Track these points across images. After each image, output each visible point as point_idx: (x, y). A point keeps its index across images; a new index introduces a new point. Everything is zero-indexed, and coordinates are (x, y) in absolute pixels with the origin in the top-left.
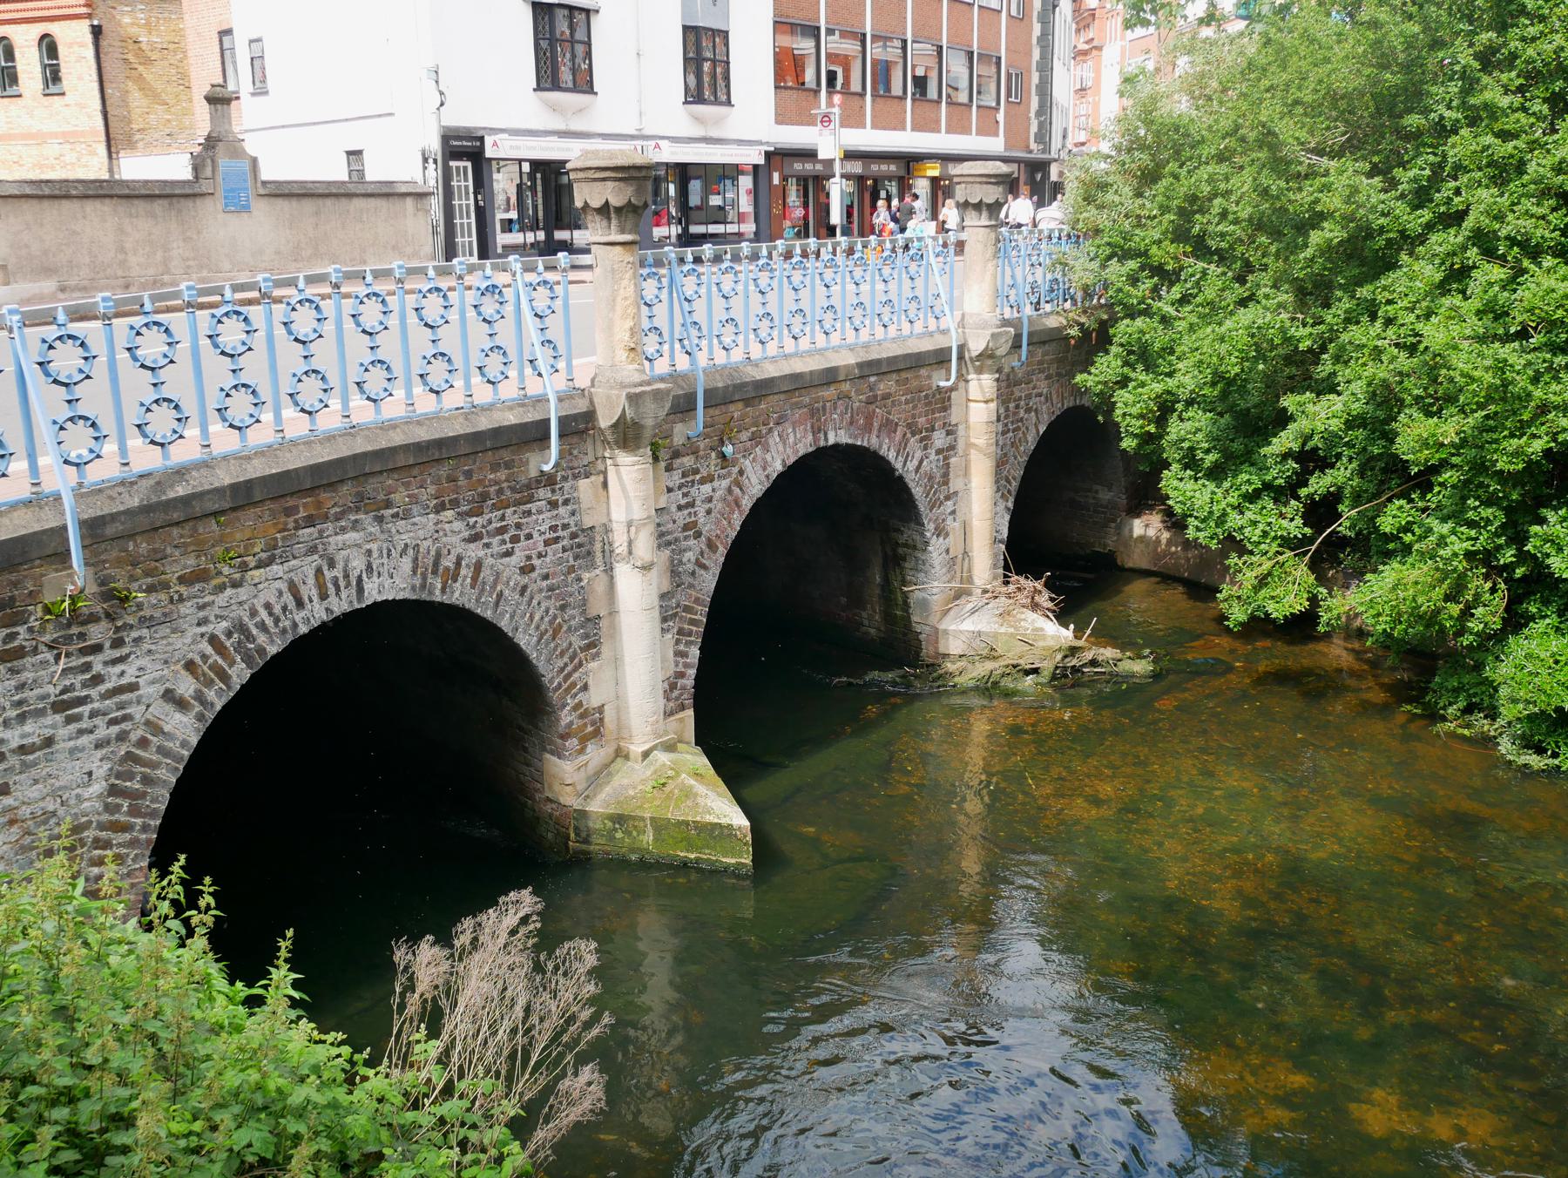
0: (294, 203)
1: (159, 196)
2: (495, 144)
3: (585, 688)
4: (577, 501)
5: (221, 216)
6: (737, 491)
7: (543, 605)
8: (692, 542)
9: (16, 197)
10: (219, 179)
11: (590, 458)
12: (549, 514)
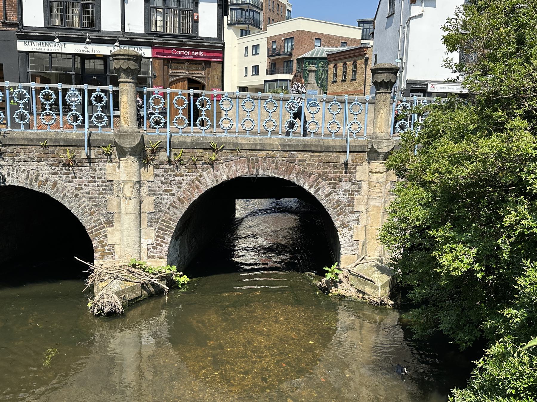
3: (106, 236)
4: (105, 170)
12: (90, 172)
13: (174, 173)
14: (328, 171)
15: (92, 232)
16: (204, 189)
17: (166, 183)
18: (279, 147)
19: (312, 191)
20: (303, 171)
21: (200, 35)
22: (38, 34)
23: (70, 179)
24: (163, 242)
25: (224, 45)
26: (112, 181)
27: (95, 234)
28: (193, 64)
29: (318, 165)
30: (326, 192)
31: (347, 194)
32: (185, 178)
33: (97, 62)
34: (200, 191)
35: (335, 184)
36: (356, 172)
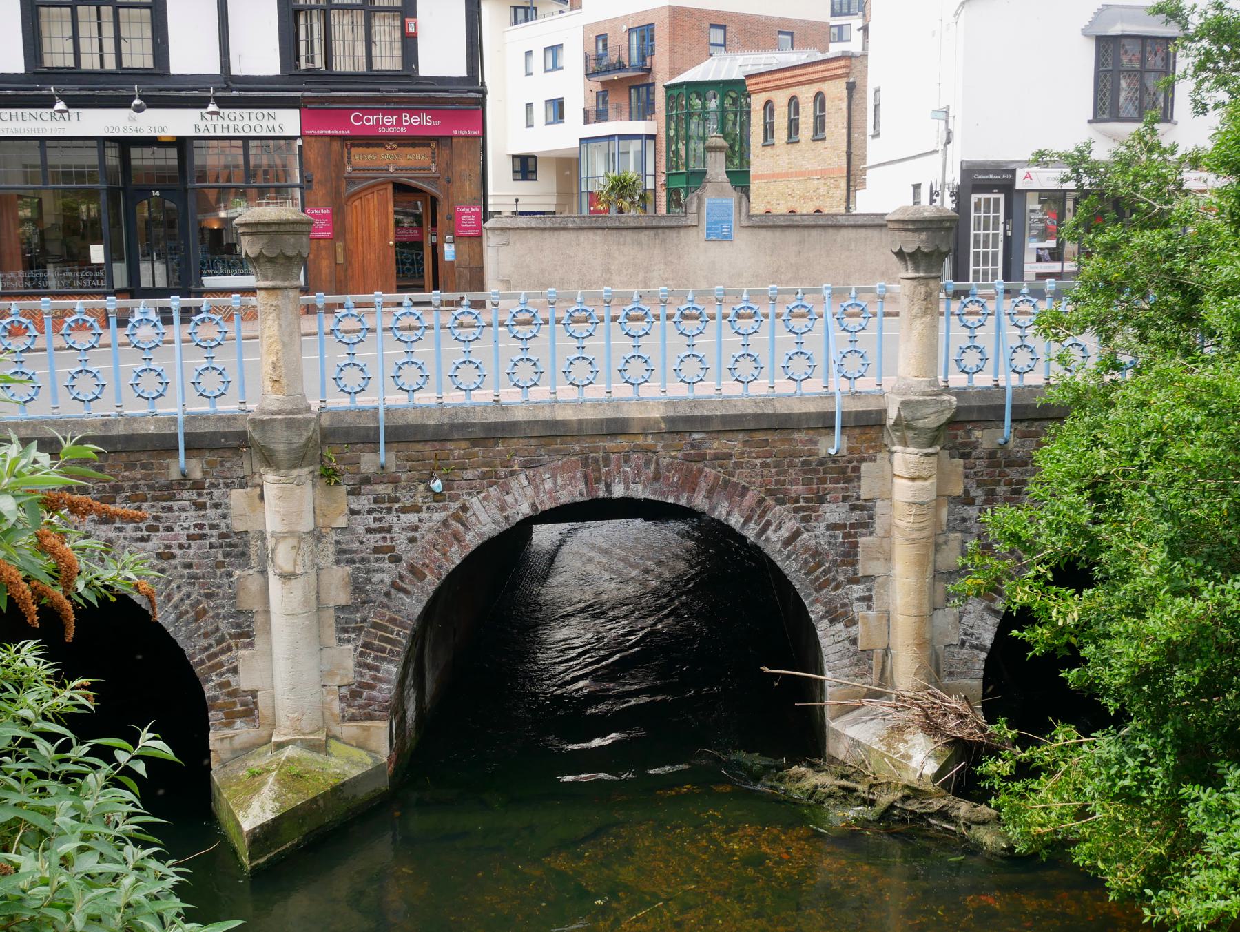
0: (778, 233)
1: (646, 228)
2: (1028, 176)
3: (235, 670)
4: (228, 507)
5: (703, 244)
6: (456, 526)
7: (184, 590)
8: (386, 565)
9: (523, 229)
10: (704, 213)
11: (247, 471)
12: (193, 513)
13: (397, 505)
14: (788, 479)
15: (202, 662)
16: (472, 541)
17: (380, 530)
18: (663, 425)
19: (750, 533)
20: (726, 482)
21: (421, 74)
22: (9, 92)
23: (145, 533)
24: (375, 678)
25: (484, 93)
26: (246, 532)
27: (210, 667)
28: (404, 145)
29: (764, 466)
30: (785, 533)
31: (839, 533)
32: (424, 515)
33: (160, 152)
34: (462, 547)
35: (807, 510)
36: (859, 478)
